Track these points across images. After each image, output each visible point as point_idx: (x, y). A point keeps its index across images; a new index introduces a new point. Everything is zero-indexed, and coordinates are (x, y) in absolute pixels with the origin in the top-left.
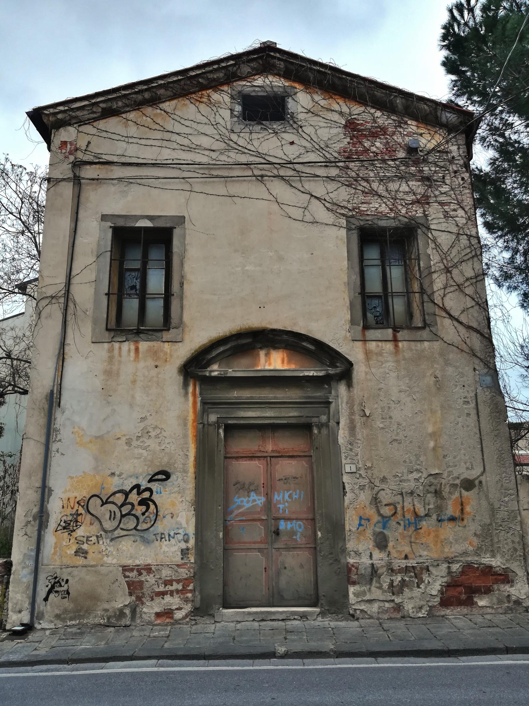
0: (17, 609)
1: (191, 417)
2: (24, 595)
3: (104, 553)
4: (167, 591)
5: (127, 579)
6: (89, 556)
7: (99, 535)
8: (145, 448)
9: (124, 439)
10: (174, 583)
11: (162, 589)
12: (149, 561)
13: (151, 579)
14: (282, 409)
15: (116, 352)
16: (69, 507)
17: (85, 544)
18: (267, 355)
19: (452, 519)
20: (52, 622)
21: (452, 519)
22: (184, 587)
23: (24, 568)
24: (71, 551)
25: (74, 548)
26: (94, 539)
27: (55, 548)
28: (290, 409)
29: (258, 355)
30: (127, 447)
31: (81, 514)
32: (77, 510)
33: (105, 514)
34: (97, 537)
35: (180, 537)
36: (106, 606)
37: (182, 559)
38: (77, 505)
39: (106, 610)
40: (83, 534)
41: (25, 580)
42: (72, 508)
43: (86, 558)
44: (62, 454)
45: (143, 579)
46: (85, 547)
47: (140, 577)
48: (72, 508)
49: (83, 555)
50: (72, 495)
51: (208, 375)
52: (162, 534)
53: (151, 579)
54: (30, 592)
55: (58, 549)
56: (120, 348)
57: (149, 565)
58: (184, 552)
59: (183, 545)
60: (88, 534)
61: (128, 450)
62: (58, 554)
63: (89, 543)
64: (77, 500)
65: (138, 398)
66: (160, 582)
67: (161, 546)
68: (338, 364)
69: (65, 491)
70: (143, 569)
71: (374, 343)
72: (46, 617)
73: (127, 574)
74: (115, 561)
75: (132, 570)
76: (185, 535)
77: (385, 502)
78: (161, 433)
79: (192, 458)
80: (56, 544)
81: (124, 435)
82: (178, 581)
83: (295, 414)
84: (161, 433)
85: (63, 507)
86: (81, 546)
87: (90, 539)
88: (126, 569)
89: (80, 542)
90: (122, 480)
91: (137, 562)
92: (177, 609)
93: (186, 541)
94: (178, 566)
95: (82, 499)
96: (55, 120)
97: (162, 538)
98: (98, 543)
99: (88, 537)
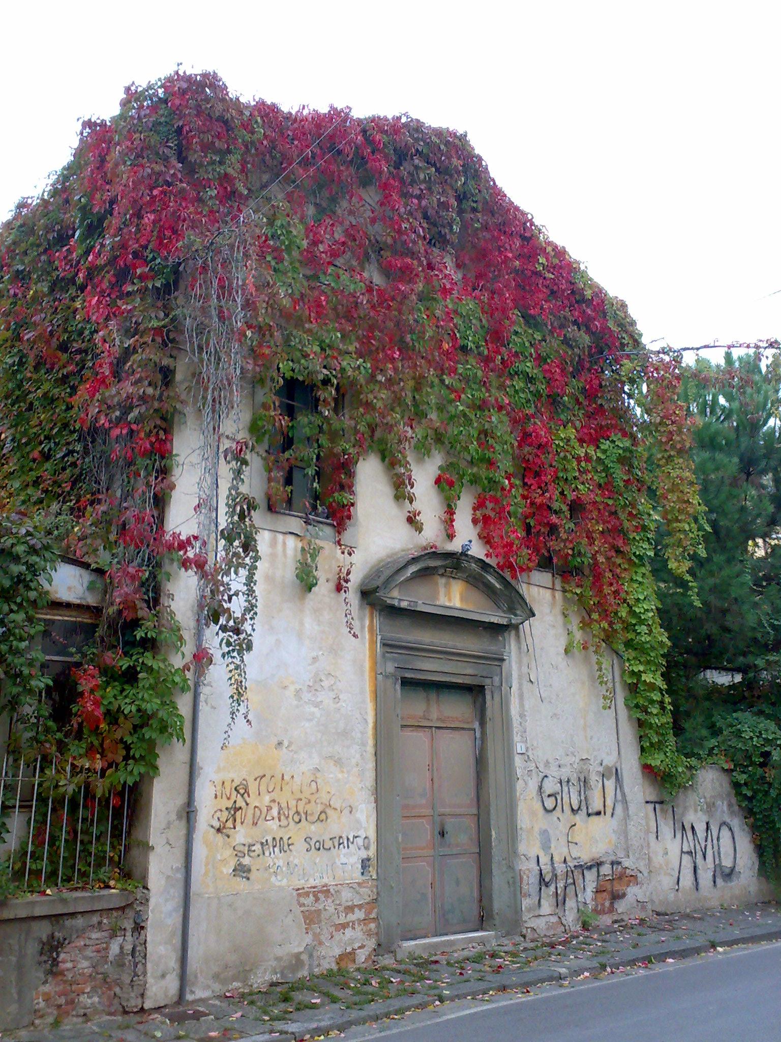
0: (159, 973)
1: (367, 665)
2: (169, 947)
3: (272, 870)
4: (348, 923)
5: (302, 909)
6: (253, 875)
7: (264, 841)
8: (317, 705)
9: (292, 688)
10: (356, 910)
11: (342, 920)
12: (325, 880)
13: (329, 906)
14: (459, 663)
15: (279, 547)
16: (224, 796)
17: (247, 857)
18: (447, 585)
19: (598, 813)
20: (208, 987)
21: (598, 813)
22: (366, 915)
23: (167, 900)
24: (228, 869)
25: (232, 864)
26: (257, 847)
27: (207, 864)
28: (466, 664)
29: (437, 584)
30: (296, 702)
31: (240, 808)
32: (235, 802)
33: (271, 808)
34: (262, 844)
35: (360, 841)
36: (279, 952)
37: (362, 874)
38: (234, 793)
39: (279, 959)
40: (243, 841)
41: (169, 921)
42: (229, 799)
43: (248, 879)
44: (213, 708)
45: (321, 907)
46: (246, 861)
47: (316, 905)
48: (229, 799)
49: (244, 875)
50: (228, 776)
51: (396, 604)
52: (341, 837)
53: (329, 906)
54: (177, 940)
55: (210, 866)
56: (284, 544)
57: (325, 885)
58: (365, 863)
59: (364, 854)
60: (250, 841)
61: (297, 707)
62: (211, 875)
63: (252, 854)
64: (235, 785)
65: (307, 625)
66: (341, 909)
67: (339, 856)
68: (518, 612)
69: (219, 770)
70: (319, 892)
71: (536, 589)
72: (201, 979)
73: (302, 900)
74: (284, 882)
75: (307, 894)
76: (366, 838)
77: (548, 793)
78: (335, 683)
79: (371, 724)
80: (207, 858)
81: (293, 683)
82: (360, 907)
83: (469, 671)
84: (335, 683)
85: (216, 797)
86: (241, 860)
87: (253, 848)
88: (301, 893)
89: (239, 854)
90: (291, 754)
91: (312, 883)
92: (360, 948)
93: (367, 848)
94: (359, 884)
95: (241, 784)
96: (638, 406)
97: (340, 844)
98: (264, 854)
99: (250, 845)
